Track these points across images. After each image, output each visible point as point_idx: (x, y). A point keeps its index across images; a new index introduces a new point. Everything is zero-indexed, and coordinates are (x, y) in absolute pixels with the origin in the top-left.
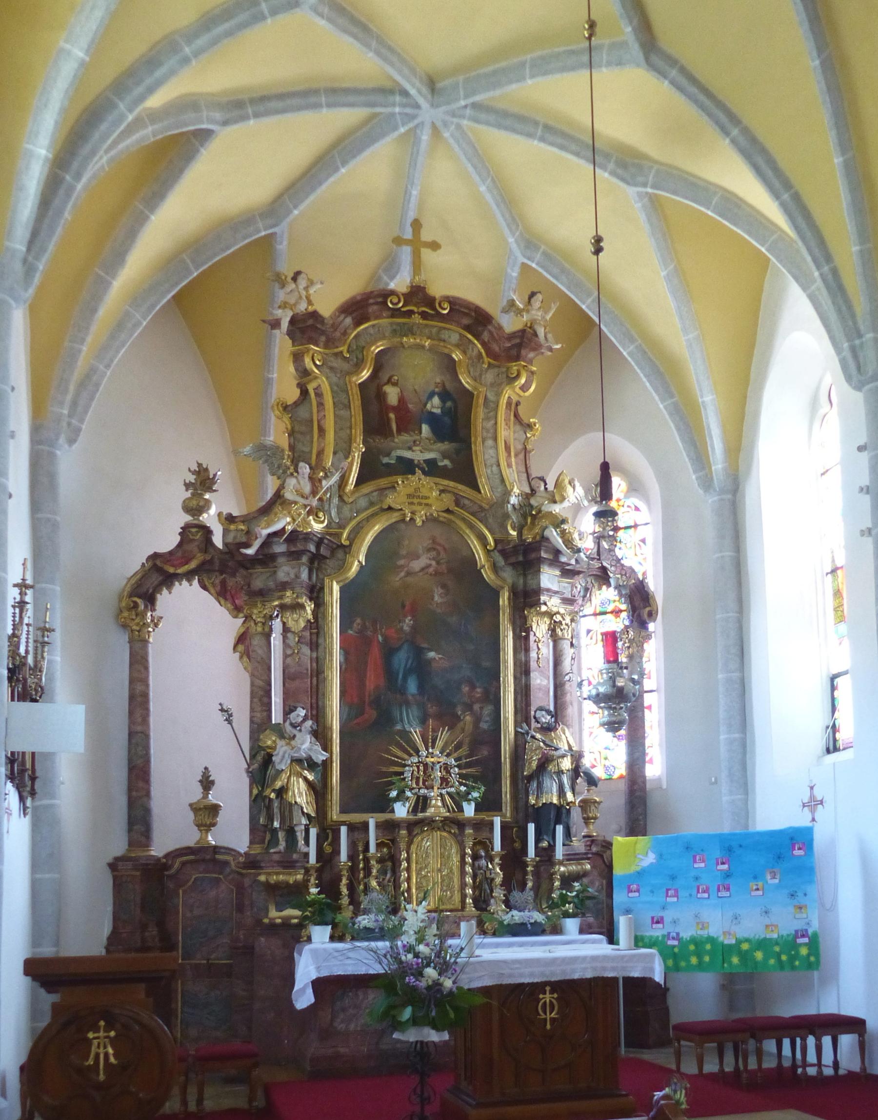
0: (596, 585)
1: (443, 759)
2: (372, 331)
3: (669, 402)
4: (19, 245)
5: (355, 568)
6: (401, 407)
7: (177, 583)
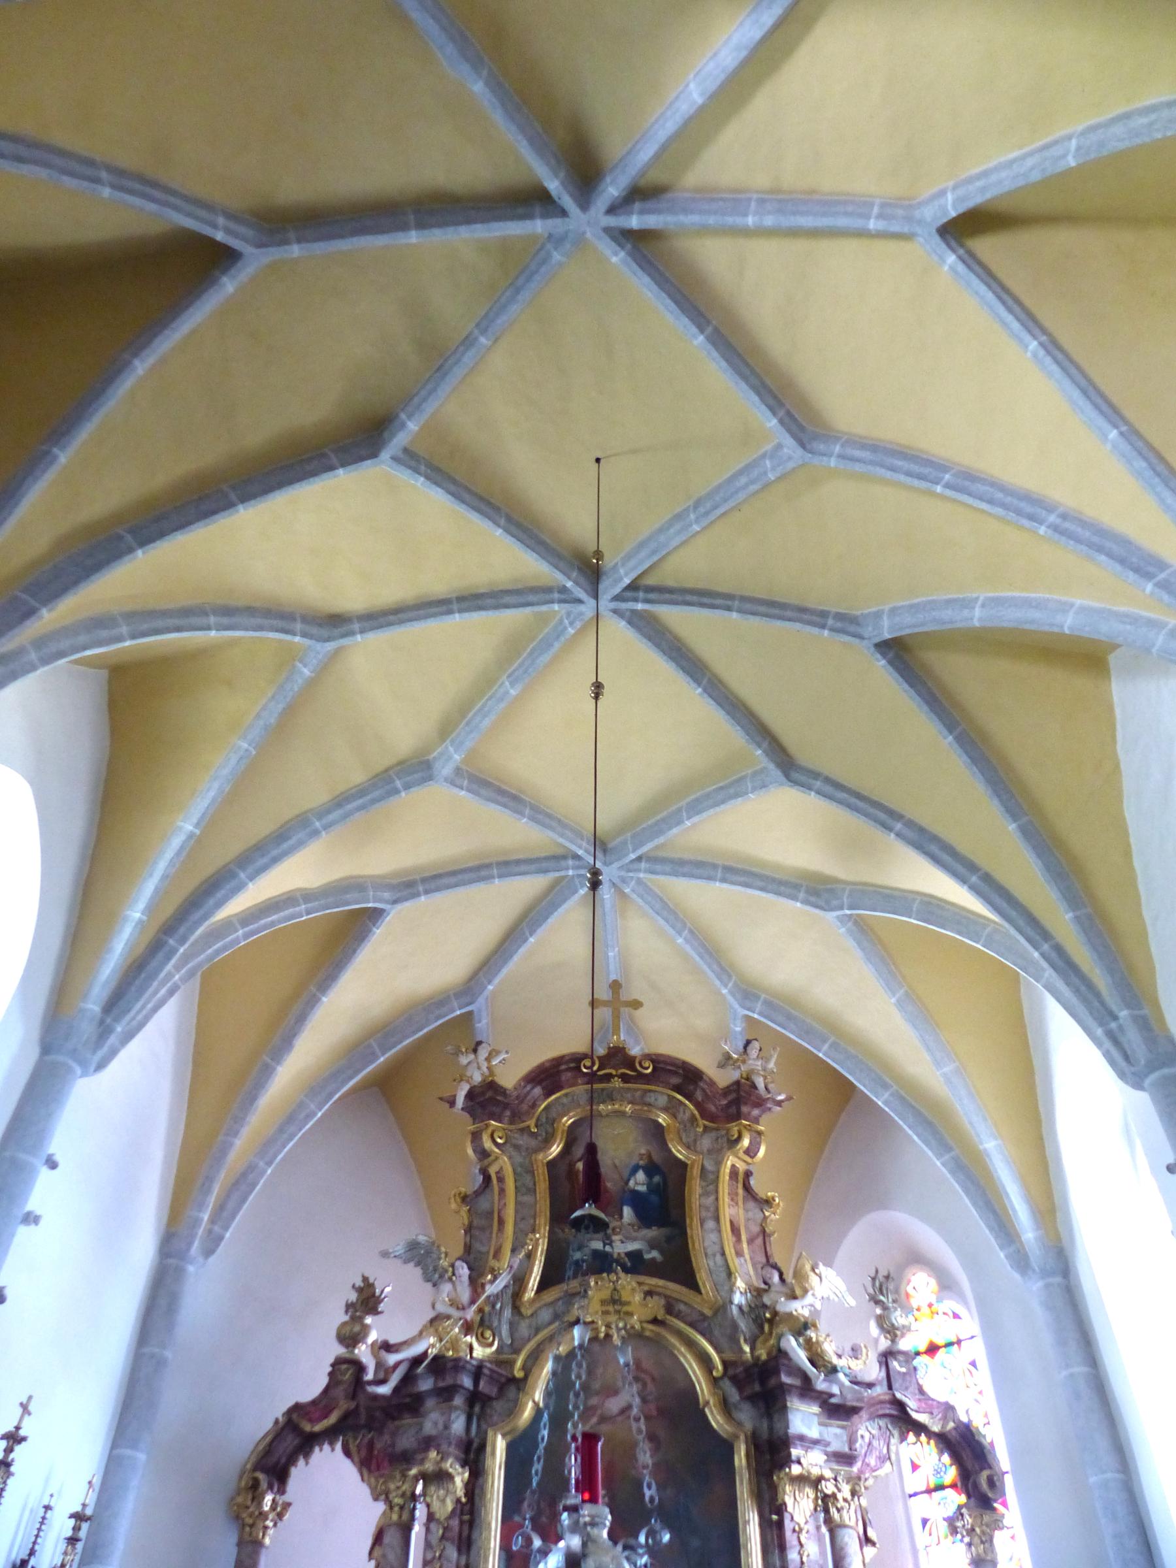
0: (896, 1433)
2: (565, 1100)
3: (947, 1157)
7: (317, 1449)
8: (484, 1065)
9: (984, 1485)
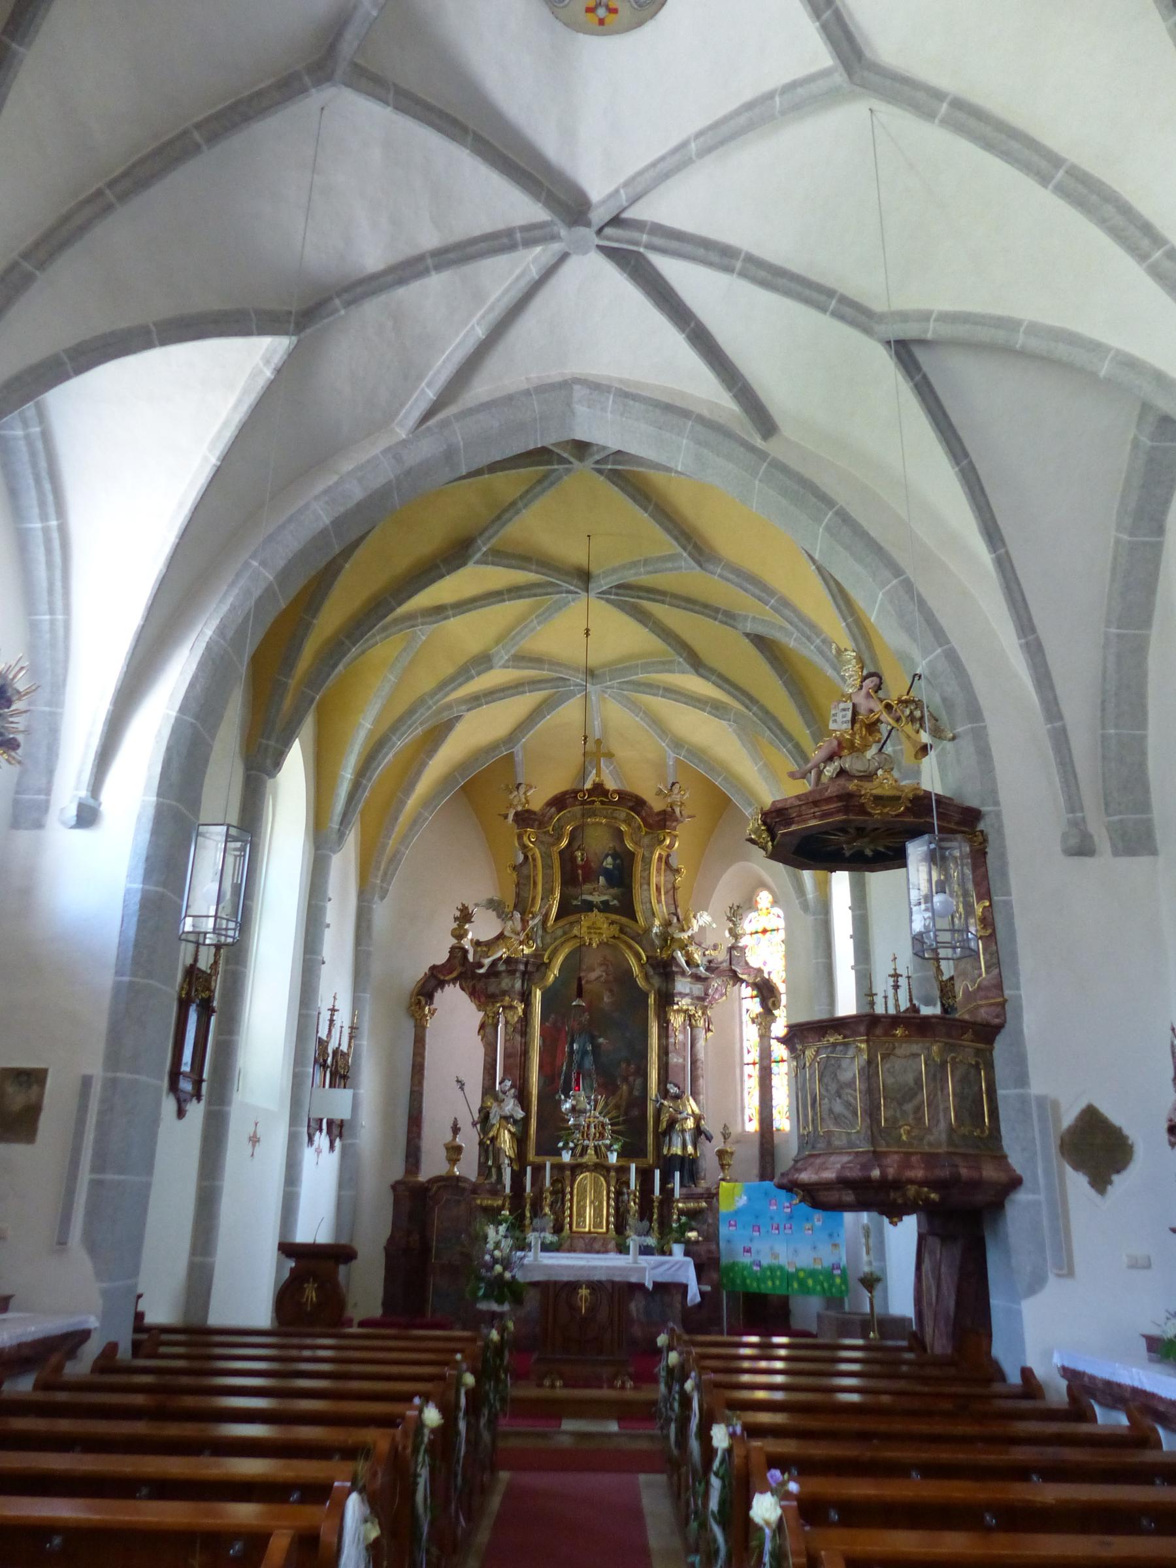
1: (601, 1119)
4: (336, 826)
6: (586, 866)
8: (523, 797)
9: (770, 1004)
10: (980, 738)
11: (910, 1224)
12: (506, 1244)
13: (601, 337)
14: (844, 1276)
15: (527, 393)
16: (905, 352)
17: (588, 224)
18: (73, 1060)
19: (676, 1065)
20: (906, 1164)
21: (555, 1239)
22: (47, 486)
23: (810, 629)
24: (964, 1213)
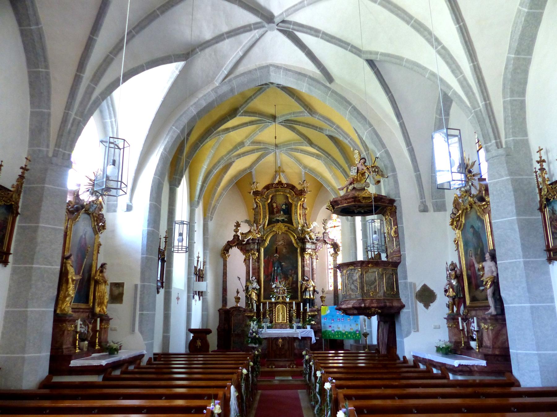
4: (197, 200)
5: (267, 244)
10: (395, 177)
11: (375, 319)
12: (256, 327)
13: (278, 51)
14: (359, 333)
15: (256, 70)
16: (371, 63)
17: (274, 23)
18: (132, 280)
19: (307, 271)
20: (372, 302)
21: (270, 325)
22: (111, 109)
23: (347, 135)
24: (390, 315)
